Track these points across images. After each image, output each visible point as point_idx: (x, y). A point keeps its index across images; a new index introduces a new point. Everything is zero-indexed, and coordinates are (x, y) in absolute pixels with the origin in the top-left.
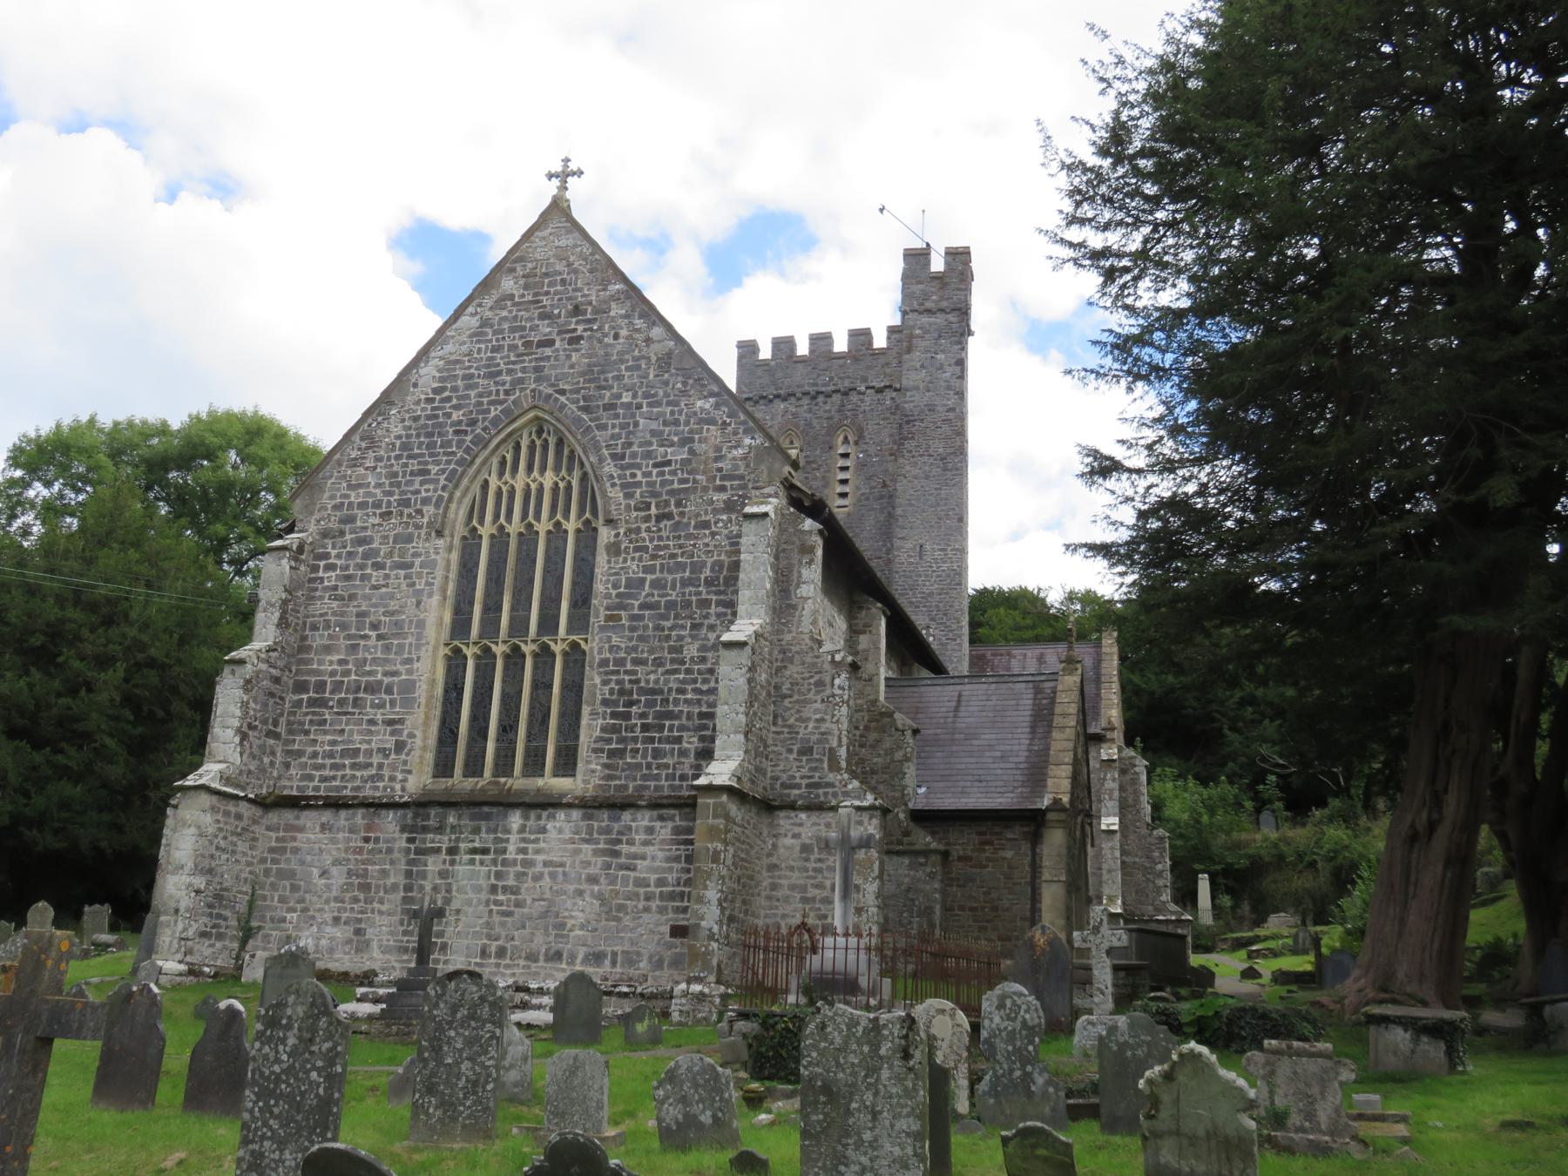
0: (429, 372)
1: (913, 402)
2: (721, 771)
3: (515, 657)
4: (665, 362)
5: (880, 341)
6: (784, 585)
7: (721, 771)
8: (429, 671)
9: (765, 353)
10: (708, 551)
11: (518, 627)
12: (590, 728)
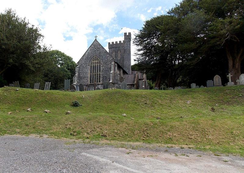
0: (87, 53)
1: (126, 48)
2: (111, 81)
3: (93, 75)
4: (105, 52)
5: (122, 42)
6: (114, 68)
7: (111, 81)
8: (89, 76)
9: (111, 44)
10: (109, 66)
11: (95, 72)
12: (101, 79)
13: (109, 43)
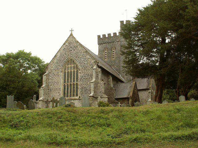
0: (59, 54)
8: (62, 88)
9: (101, 37)
11: (71, 81)
13: (99, 36)
